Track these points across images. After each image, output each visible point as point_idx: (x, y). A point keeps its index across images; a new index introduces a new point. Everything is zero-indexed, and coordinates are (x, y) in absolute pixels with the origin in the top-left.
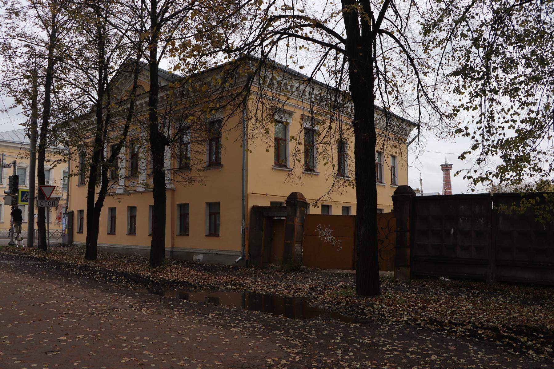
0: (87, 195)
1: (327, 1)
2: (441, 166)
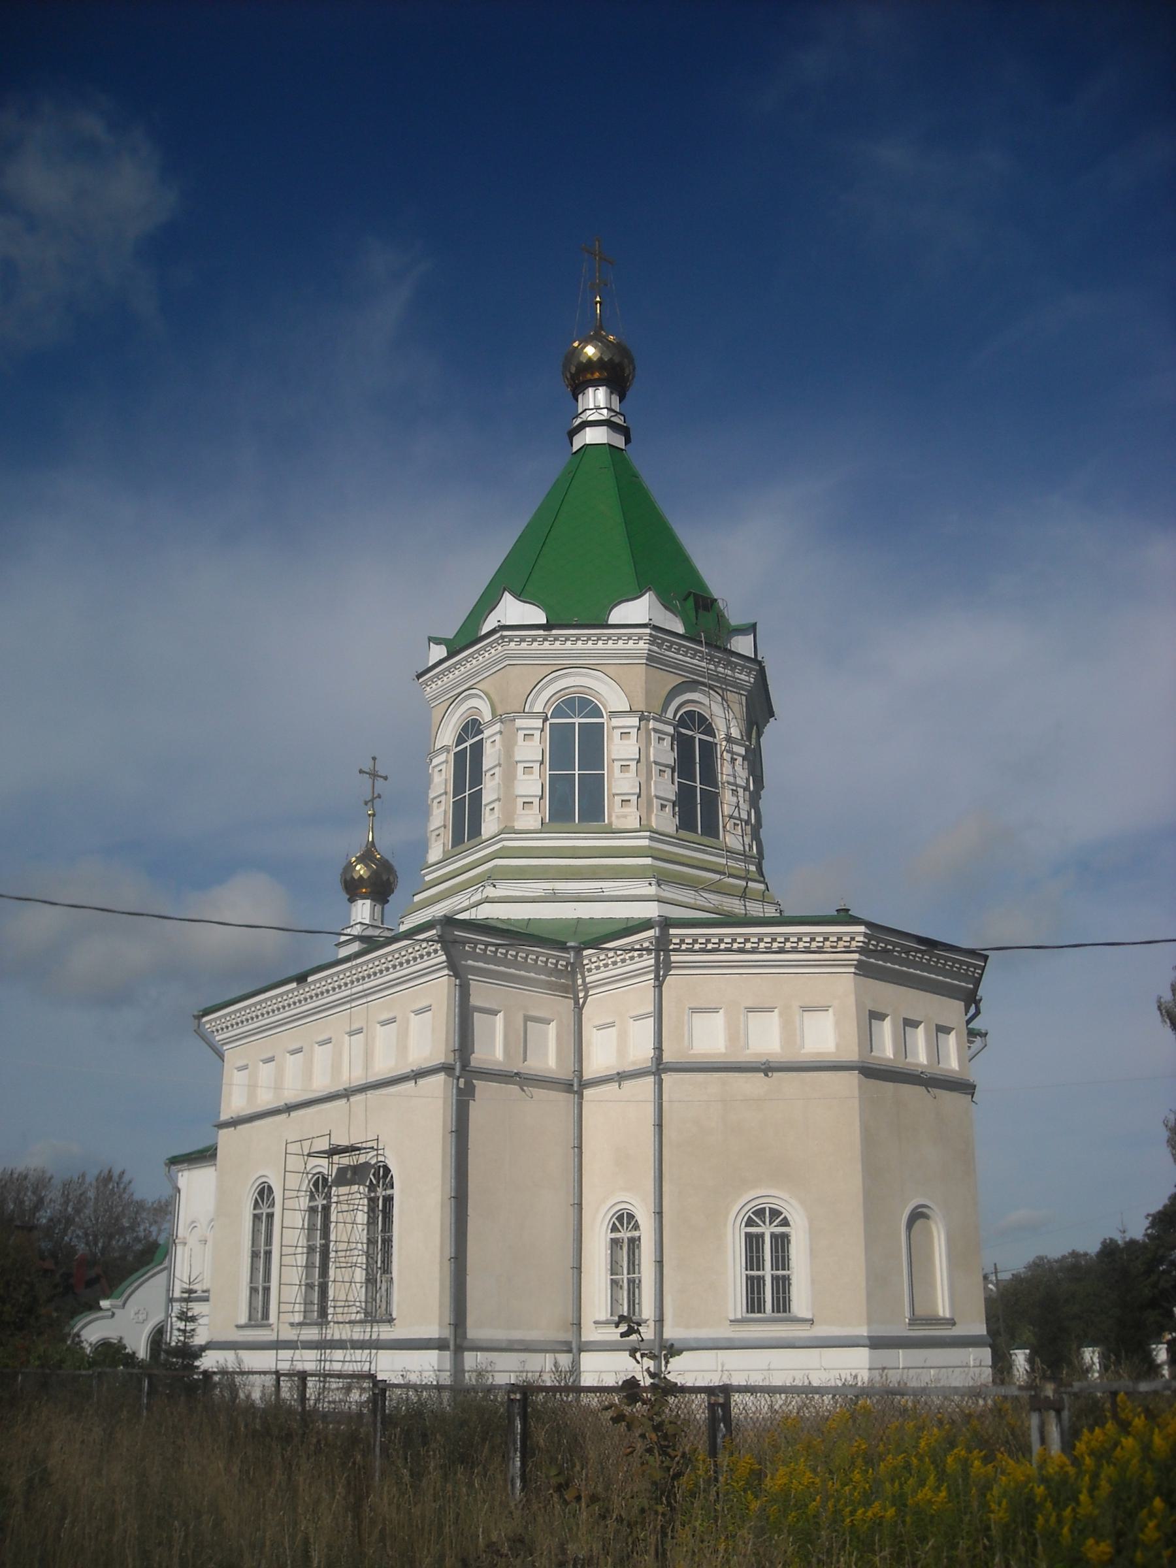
0: (469, 1218)
1: (1174, 940)
2: (756, 623)
